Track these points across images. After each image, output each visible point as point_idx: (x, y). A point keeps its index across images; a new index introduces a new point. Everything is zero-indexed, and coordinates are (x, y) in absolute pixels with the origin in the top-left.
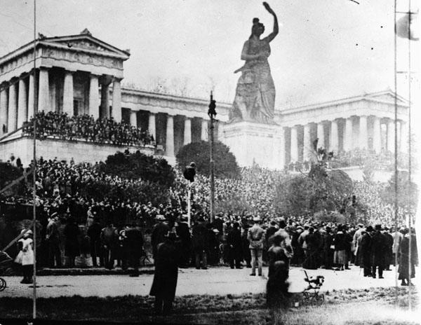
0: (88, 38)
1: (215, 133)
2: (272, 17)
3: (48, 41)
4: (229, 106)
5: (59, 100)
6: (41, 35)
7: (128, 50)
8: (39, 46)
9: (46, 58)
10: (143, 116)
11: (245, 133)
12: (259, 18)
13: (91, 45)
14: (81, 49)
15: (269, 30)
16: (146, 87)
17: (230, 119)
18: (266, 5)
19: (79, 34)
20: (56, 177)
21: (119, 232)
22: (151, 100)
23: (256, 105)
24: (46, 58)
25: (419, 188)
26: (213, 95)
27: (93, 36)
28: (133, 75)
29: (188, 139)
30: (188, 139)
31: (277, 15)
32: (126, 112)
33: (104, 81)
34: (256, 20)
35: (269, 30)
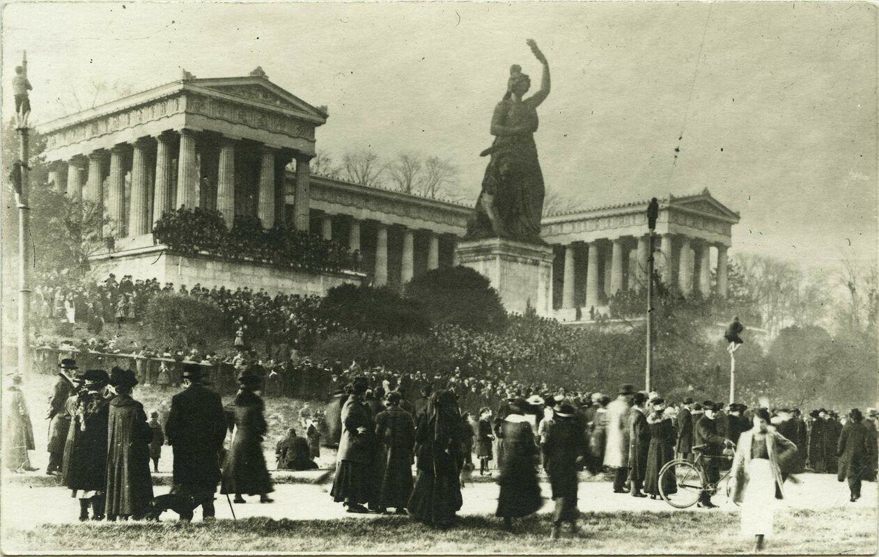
0: (262, 84)
1: (127, 206)
2: (540, 66)
3: (198, 85)
4: (470, 212)
5: (209, 191)
6: (187, 74)
7: (325, 108)
8: (182, 93)
9: (192, 114)
10: (342, 223)
11: (498, 257)
12: (522, 66)
13: (265, 96)
14: (250, 103)
15: (535, 87)
16: (87, 104)
17: (470, 231)
18: (533, 45)
19: (246, 74)
20: (173, 330)
21: (458, 381)
22: (422, 210)
23: (514, 211)
24: (192, 114)
25: (4, 463)
26: (31, 77)
27: (271, 80)
28: (332, 149)
29: (434, 263)
30: (434, 263)
31: (551, 66)
32: (316, 218)
33: (283, 155)
34: (516, 69)
35: (535, 87)
